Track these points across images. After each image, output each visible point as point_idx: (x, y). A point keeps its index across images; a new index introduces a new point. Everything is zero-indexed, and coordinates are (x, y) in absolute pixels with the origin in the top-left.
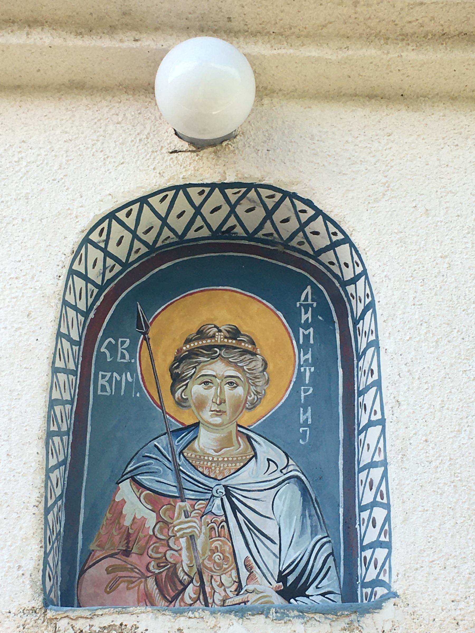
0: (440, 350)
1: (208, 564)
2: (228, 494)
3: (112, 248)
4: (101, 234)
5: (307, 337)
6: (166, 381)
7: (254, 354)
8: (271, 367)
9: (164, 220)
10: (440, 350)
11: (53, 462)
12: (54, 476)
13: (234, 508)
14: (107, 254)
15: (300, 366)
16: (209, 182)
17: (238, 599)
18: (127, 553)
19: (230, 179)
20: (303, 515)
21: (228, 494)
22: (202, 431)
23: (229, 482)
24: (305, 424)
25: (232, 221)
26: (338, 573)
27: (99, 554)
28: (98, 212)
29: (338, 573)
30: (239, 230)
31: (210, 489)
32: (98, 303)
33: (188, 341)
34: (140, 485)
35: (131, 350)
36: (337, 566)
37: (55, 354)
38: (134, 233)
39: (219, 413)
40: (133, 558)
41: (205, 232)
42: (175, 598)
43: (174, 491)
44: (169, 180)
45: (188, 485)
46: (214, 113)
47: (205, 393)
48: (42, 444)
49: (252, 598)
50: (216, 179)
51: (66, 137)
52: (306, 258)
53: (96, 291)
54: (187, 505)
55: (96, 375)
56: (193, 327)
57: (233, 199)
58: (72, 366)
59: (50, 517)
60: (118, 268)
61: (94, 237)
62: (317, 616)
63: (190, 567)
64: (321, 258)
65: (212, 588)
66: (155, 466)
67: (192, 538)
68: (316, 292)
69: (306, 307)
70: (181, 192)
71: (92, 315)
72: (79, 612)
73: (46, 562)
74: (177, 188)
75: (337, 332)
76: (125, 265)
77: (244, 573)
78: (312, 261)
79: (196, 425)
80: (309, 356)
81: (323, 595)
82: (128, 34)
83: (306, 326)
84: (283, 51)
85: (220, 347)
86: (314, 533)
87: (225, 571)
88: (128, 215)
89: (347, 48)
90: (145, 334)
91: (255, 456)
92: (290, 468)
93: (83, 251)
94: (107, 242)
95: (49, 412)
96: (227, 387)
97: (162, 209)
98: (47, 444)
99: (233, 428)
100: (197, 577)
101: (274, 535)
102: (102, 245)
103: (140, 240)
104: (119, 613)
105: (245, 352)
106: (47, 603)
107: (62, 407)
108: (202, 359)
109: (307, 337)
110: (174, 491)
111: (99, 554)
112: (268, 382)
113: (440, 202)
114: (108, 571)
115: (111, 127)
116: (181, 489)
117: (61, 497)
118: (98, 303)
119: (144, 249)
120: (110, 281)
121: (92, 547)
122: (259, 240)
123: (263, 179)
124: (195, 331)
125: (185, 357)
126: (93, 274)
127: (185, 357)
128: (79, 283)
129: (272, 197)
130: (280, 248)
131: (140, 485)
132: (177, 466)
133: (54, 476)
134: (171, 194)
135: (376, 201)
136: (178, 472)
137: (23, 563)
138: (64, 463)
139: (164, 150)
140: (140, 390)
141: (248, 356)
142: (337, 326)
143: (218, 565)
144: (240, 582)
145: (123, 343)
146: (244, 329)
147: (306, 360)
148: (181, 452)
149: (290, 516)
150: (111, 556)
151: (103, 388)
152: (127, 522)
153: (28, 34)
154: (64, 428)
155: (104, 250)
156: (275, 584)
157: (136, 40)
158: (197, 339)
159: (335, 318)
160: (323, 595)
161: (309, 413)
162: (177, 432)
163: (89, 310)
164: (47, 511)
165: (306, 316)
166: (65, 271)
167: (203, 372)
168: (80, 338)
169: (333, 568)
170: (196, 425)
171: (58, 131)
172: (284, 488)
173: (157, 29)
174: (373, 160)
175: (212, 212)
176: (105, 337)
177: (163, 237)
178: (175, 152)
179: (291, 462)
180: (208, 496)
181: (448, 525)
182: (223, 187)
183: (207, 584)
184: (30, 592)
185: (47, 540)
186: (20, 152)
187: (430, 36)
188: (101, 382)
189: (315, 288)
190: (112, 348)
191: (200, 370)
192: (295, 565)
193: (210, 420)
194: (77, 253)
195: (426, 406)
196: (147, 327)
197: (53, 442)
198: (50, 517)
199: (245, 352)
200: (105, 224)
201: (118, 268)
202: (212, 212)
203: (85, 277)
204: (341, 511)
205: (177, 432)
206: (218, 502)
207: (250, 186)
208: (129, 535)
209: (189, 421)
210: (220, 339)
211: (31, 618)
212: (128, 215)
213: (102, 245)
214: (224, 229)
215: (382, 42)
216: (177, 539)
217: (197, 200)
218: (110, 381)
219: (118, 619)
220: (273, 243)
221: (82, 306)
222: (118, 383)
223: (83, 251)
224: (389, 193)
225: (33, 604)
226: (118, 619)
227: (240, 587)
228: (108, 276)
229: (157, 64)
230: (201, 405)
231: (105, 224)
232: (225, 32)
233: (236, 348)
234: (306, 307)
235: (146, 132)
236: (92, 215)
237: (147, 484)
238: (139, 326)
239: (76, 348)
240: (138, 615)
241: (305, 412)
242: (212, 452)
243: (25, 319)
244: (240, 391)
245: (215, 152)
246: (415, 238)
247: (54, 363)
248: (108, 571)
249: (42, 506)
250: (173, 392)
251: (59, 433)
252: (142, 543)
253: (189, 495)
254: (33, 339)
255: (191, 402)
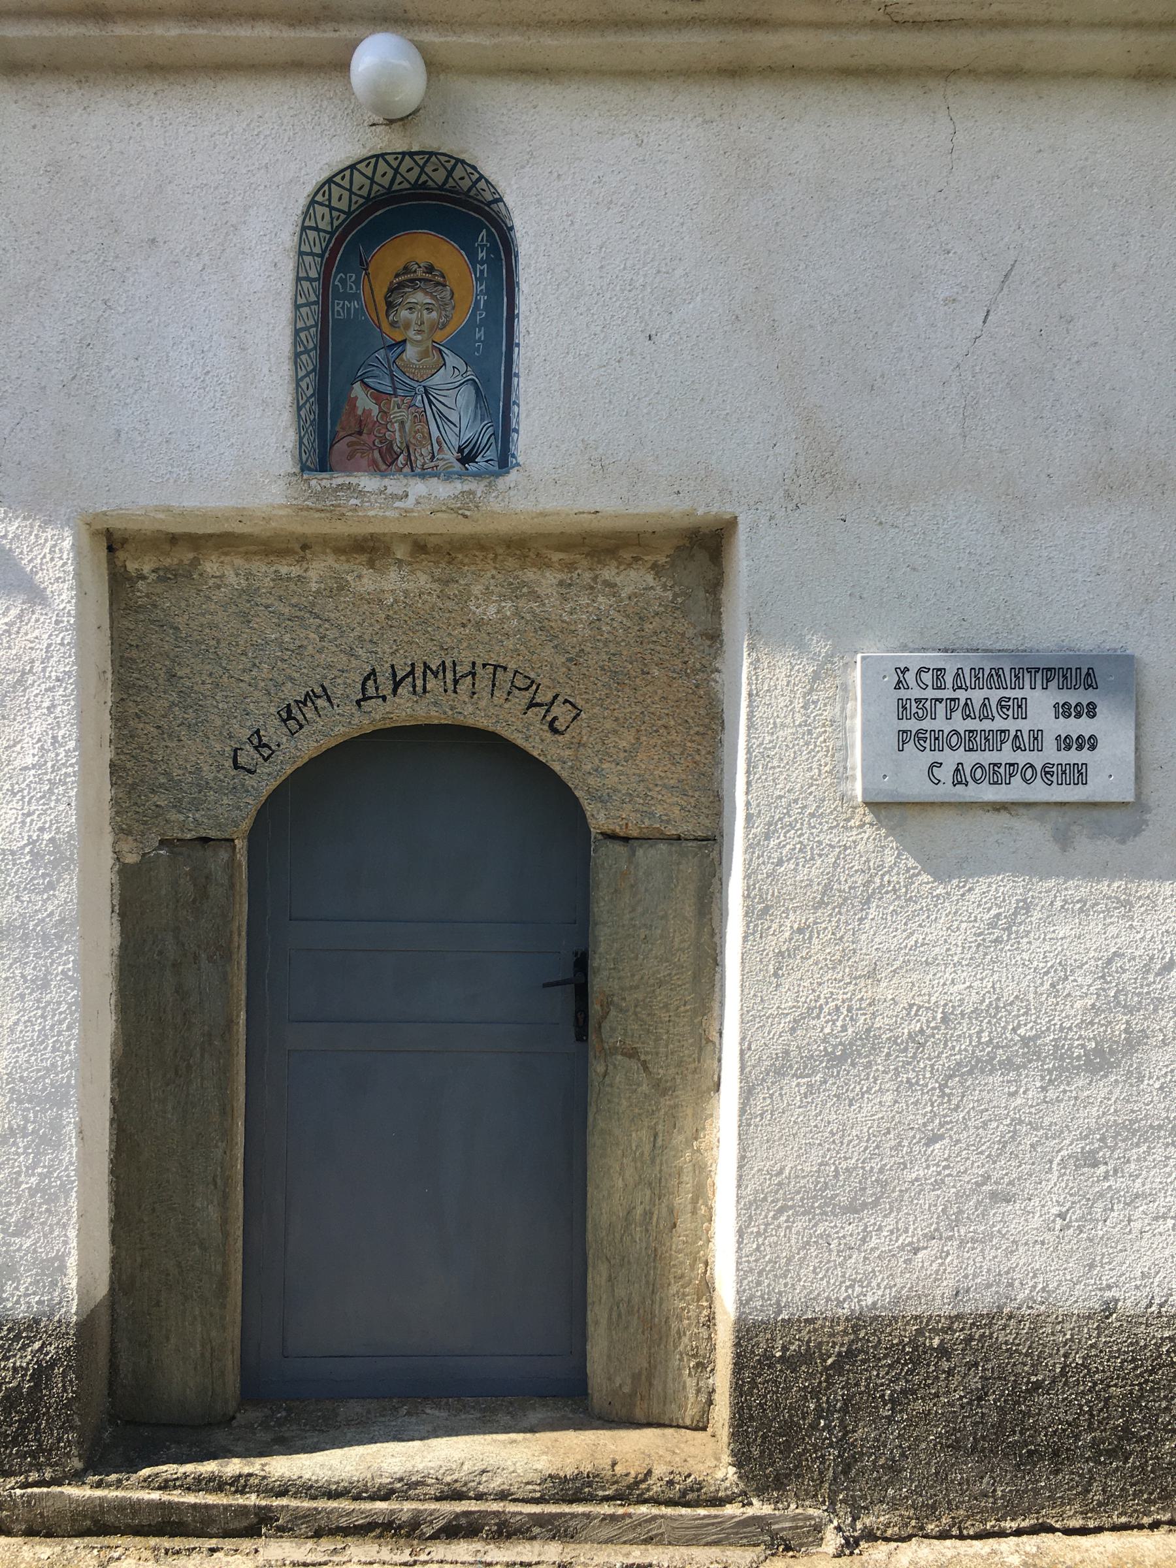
0: (560, 291)
1: (413, 441)
2: (426, 392)
3: (335, 203)
4: (324, 195)
5: (482, 272)
6: (383, 307)
7: (445, 286)
8: (456, 296)
9: (372, 180)
10: (560, 291)
11: (301, 374)
12: (303, 384)
13: (430, 402)
14: (332, 209)
15: (477, 295)
16: (400, 150)
17: (432, 464)
18: (360, 433)
19: (415, 149)
20: (476, 407)
21: (426, 392)
22: (408, 346)
23: (427, 383)
24: (479, 340)
25: (424, 178)
26: (497, 447)
27: (342, 434)
28: (319, 180)
29: (497, 447)
30: (430, 183)
31: (414, 388)
32: (331, 245)
33: (397, 276)
34: (367, 385)
35: (357, 282)
36: (496, 442)
37: (296, 296)
38: (350, 190)
39: (420, 332)
40: (365, 437)
41: (406, 185)
42: (392, 464)
43: (390, 390)
44: (369, 151)
45: (399, 386)
46: (397, 99)
47: (409, 316)
48: (292, 363)
49: (441, 463)
50: (404, 148)
51: (292, 112)
52: (482, 205)
53: (328, 236)
54: (398, 399)
55: (333, 303)
56: (400, 265)
57: (421, 163)
58: (313, 298)
59: (302, 413)
60: (343, 216)
61: (319, 198)
62: (469, 478)
63: (401, 443)
64: (492, 206)
65: (416, 457)
66: (377, 372)
67: (402, 423)
68: (490, 234)
69: (482, 247)
70: (380, 159)
71: (327, 255)
72: (324, 475)
73: (301, 443)
74: (377, 156)
75: (504, 267)
76: (348, 214)
77: (436, 447)
78: (486, 208)
79: (404, 341)
80: (483, 287)
81: (487, 461)
82: (329, 24)
83: (482, 263)
84: (449, 39)
85: (420, 280)
86: (482, 420)
87: (424, 446)
88: (343, 178)
89: (498, 34)
90: (366, 270)
91: (445, 364)
92: (468, 373)
93: (311, 211)
94: (330, 200)
95: (295, 339)
96: (425, 312)
97: (369, 172)
98: (296, 363)
99: (430, 343)
100: (406, 450)
101: (456, 422)
102: (327, 203)
103: (356, 194)
104: (348, 476)
105: (438, 284)
106: (304, 468)
107: (306, 332)
108: (407, 290)
109: (482, 272)
110: (390, 390)
111: (342, 434)
112: (454, 308)
113: (569, 168)
114: (349, 445)
115: (325, 103)
116: (395, 389)
117: (312, 395)
118: (331, 245)
119: (361, 201)
120: (338, 227)
121: (338, 428)
122: (447, 190)
123: (440, 148)
124: (402, 267)
125: (396, 288)
126: (322, 225)
127: (396, 288)
128: (312, 234)
129: (448, 161)
130: (463, 197)
131: (367, 385)
132: (391, 371)
133: (303, 384)
134: (373, 161)
135: (523, 167)
136: (392, 376)
137: (286, 444)
138: (314, 370)
139: (366, 124)
140: (364, 314)
141: (440, 288)
142: (504, 262)
143: (420, 442)
144: (433, 453)
145: (351, 277)
146: (437, 266)
147: (481, 290)
148: (394, 362)
149: (467, 407)
150: (350, 435)
151: (339, 314)
152: (359, 412)
153: (253, 27)
154: (311, 345)
155: (329, 206)
156: (456, 454)
157: (335, 31)
158: (404, 274)
159: (503, 257)
160: (487, 461)
161: (482, 332)
162: (391, 347)
163: (324, 252)
164: (299, 408)
165: (482, 255)
166: (298, 229)
167: (408, 301)
168: (319, 274)
169: (494, 444)
170: (404, 341)
171: (286, 107)
172: (463, 388)
173: (351, 20)
174: (522, 130)
175: (408, 171)
176: (337, 273)
177: (373, 192)
178: (374, 125)
179: (469, 369)
180: (413, 394)
181: (554, 419)
182: (411, 154)
183: (412, 454)
184: (291, 463)
185: (300, 428)
186: (258, 126)
187: (561, 23)
188: (336, 308)
189: (488, 230)
190: (343, 281)
191: (407, 298)
192: (469, 442)
193: (415, 337)
194: (306, 214)
195: (546, 335)
196: (367, 264)
197: (301, 360)
198: (302, 413)
199: (438, 284)
200: (326, 188)
201: (343, 216)
202: (408, 171)
203: (316, 229)
204: (501, 404)
205: (391, 347)
206: (419, 397)
207: (431, 154)
208: (361, 421)
209: (399, 339)
210: (420, 273)
211: (294, 479)
212: (343, 178)
213: (327, 203)
214: (420, 182)
215: (525, 28)
216: (393, 424)
217: (395, 164)
218: (343, 308)
219: (347, 480)
220: (457, 193)
221: (317, 250)
222: (349, 309)
223: (311, 211)
224: (531, 161)
225: (294, 470)
226: (347, 480)
227: (433, 456)
228: (336, 223)
229: (354, 48)
230: (407, 326)
231: (326, 188)
232: (403, 21)
233: (431, 281)
234: (482, 247)
235: (352, 106)
236: (314, 182)
237: (372, 385)
238: (362, 264)
239: (315, 284)
240: (359, 477)
241: (480, 331)
242: (415, 361)
243: (273, 269)
244: (434, 314)
245: (403, 125)
246: (549, 200)
247: (296, 301)
248: (349, 445)
249: (295, 406)
250: (387, 316)
251: (307, 352)
252: (370, 426)
253: (400, 392)
254: (280, 284)
255: (400, 324)
